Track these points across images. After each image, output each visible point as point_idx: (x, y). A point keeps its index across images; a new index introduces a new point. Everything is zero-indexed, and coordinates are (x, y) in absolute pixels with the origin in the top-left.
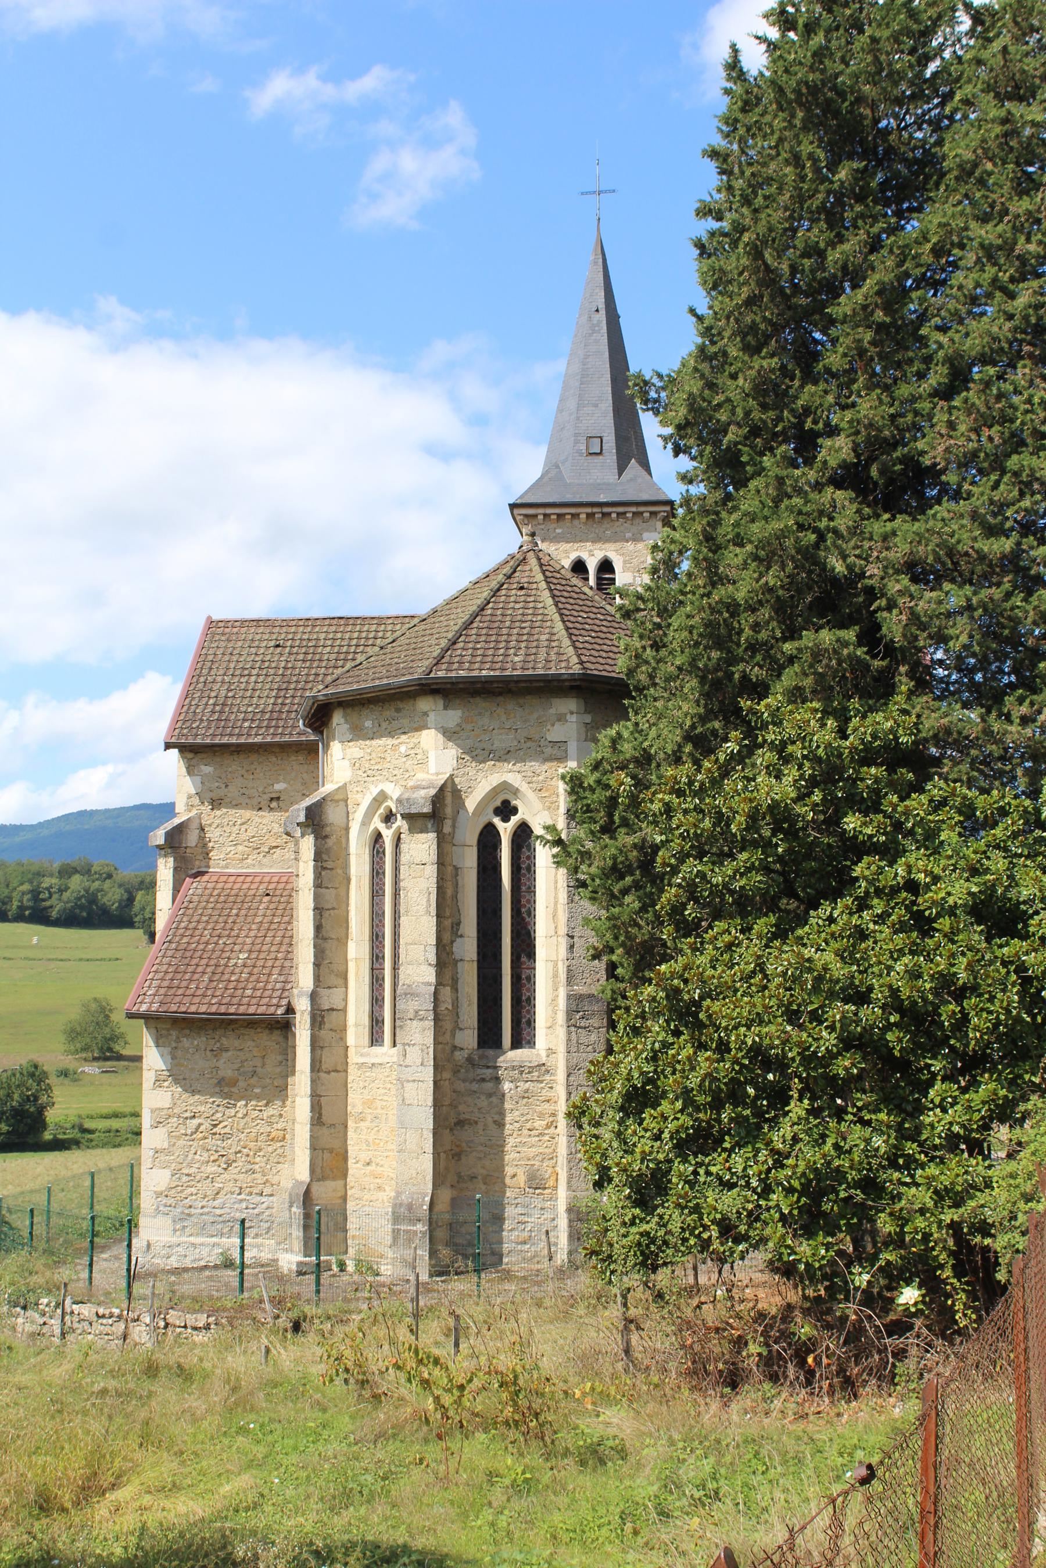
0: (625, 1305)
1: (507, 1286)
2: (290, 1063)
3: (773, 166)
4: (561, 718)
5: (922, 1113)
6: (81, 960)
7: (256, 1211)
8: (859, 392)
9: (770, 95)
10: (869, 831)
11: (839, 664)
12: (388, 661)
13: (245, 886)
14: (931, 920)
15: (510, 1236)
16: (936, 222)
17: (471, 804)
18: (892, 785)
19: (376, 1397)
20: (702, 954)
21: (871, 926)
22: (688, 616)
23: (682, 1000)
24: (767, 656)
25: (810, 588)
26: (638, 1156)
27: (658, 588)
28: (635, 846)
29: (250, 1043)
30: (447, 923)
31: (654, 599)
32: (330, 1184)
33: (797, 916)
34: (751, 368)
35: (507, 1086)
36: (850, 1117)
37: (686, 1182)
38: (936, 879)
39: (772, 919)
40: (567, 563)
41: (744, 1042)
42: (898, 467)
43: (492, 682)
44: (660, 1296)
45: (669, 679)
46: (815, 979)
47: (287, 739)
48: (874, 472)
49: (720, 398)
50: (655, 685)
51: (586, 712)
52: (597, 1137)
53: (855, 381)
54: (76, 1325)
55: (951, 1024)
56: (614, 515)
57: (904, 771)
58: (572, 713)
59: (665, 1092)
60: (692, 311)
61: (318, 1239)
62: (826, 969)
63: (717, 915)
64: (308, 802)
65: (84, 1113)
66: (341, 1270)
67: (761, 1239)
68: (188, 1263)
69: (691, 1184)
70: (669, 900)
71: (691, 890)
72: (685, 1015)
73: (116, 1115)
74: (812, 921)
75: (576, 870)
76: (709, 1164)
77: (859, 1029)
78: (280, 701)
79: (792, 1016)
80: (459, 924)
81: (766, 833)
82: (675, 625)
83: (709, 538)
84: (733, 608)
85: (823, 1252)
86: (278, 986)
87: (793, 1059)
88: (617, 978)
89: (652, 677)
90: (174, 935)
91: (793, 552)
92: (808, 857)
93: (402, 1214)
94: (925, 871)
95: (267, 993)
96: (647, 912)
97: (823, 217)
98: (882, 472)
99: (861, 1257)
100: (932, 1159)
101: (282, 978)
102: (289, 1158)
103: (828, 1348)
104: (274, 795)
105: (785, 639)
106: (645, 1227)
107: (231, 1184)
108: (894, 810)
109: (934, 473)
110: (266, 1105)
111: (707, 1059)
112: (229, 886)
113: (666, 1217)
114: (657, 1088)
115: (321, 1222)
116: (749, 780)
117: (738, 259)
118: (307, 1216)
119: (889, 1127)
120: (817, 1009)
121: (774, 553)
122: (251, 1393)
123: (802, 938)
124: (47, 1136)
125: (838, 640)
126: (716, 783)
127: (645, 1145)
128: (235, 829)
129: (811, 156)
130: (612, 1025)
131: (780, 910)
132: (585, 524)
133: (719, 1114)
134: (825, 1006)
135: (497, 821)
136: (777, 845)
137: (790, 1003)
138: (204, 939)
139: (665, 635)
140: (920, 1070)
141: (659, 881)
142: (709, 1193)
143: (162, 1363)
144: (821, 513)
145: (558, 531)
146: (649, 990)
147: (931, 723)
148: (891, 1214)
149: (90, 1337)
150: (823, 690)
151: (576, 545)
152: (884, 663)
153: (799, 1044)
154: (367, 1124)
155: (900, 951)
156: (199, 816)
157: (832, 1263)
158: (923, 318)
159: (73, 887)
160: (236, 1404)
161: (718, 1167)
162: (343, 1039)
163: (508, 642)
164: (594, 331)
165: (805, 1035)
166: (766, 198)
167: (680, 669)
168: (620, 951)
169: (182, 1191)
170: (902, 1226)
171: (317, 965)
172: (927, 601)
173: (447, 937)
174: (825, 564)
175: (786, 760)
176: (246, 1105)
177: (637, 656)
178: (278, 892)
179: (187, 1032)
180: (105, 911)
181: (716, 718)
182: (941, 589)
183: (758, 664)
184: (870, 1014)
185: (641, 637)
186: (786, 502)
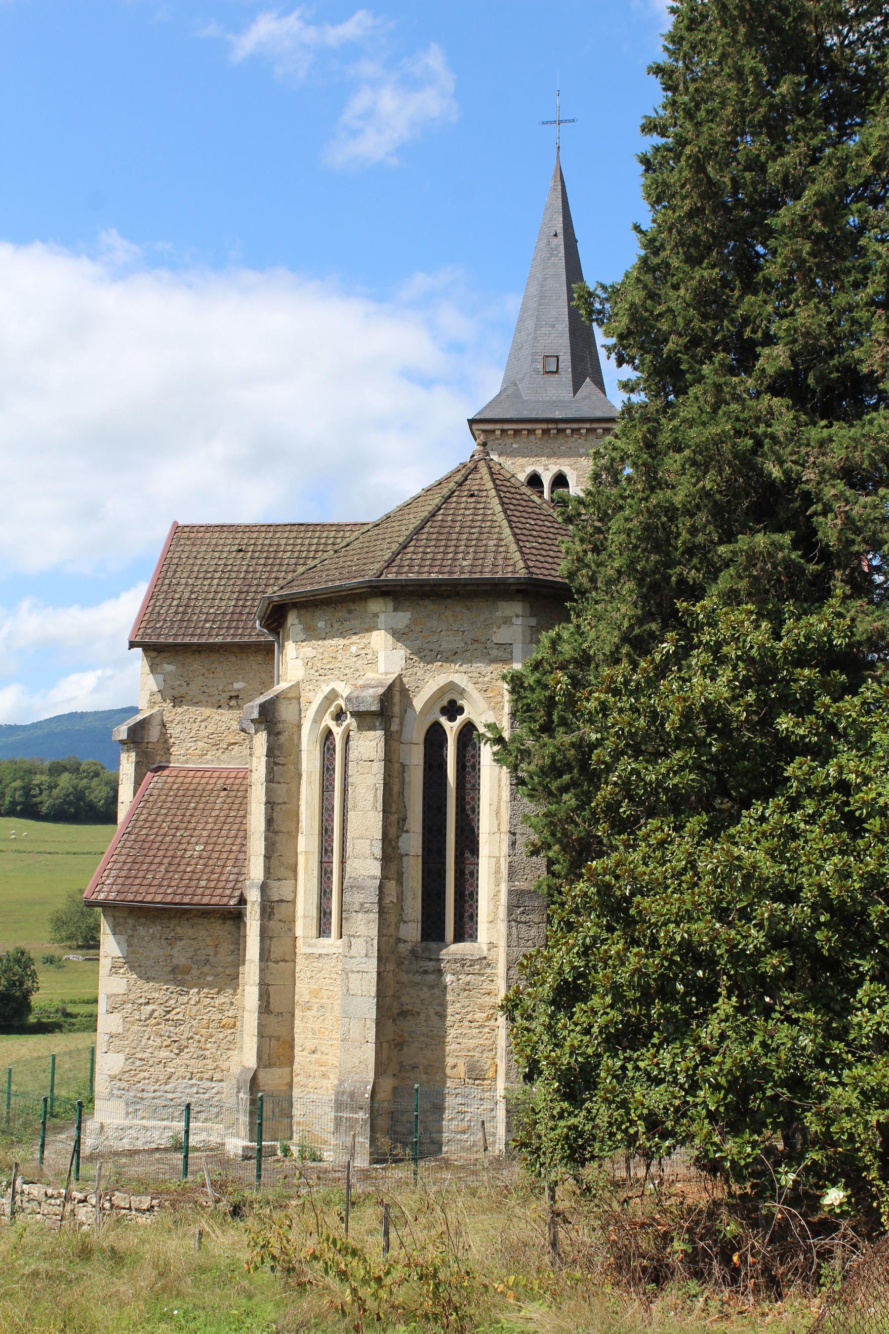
0: (552, 1198)
2: (241, 953)
3: (716, 82)
4: (507, 621)
5: (850, 1013)
6: (68, 853)
7: (206, 1096)
8: (797, 300)
9: (714, 12)
10: (801, 731)
11: (775, 566)
12: (341, 564)
13: (204, 781)
14: (862, 821)
15: (450, 1124)
16: (877, 135)
17: (418, 703)
18: (826, 687)
19: (301, 1285)
20: (635, 850)
21: (802, 825)
22: (627, 520)
23: (613, 896)
24: (704, 558)
25: (748, 495)
26: (567, 1050)
27: (598, 492)
28: (573, 744)
29: (203, 932)
30: (394, 818)
31: (594, 503)
32: (277, 1071)
33: (731, 816)
34: (692, 278)
35: (449, 978)
36: (777, 1015)
37: (614, 1077)
38: (867, 780)
40: (522, 477)
41: (674, 939)
42: (835, 375)
43: (440, 585)
45: (609, 582)
46: (744, 877)
47: (246, 639)
48: (811, 381)
49: (663, 308)
50: (596, 588)
51: (531, 615)
52: (528, 1030)
53: (794, 290)
54: (25, 1205)
55: (880, 925)
56: (569, 432)
57: (836, 672)
58: (517, 616)
59: (594, 986)
60: (637, 228)
61: (260, 1124)
62: (754, 867)
64: (262, 699)
65: (67, 998)
66: (286, 1156)
67: (687, 1136)
68: (139, 1145)
69: (619, 1079)
70: (604, 798)
71: (625, 785)
72: (617, 911)
74: (745, 820)
76: (637, 1059)
77: (787, 928)
78: (241, 603)
79: (721, 914)
80: (404, 819)
82: (614, 528)
83: (649, 446)
84: (671, 512)
85: (749, 1150)
86: (232, 877)
87: (721, 956)
89: (593, 579)
90: (134, 827)
91: (730, 457)
92: (741, 757)
94: (856, 772)
95: (222, 884)
96: (585, 810)
97: (764, 130)
98: (819, 379)
99: (792, 1157)
100: (859, 1059)
101: (236, 870)
102: (238, 1045)
103: (753, 1247)
104: (233, 694)
105: (721, 542)
106: (573, 1121)
107: (182, 1069)
108: (827, 711)
109: (872, 380)
110: (218, 993)
111: (636, 955)
112: (188, 780)
113: (594, 1111)
114: (588, 982)
115: (266, 1107)
116: (685, 681)
117: (680, 172)
118: (253, 1102)
119: (816, 1026)
120: (746, 907)
121: (711, 458)
122: (179, 1278)
123: (734, 837)
124: (32, 1019)
125: (773, 543)
126: (651, 684)
127: (574, 1039)
128: (195, 726)
129: (753, 71)
131: (715, 809)
132: (541, 439)
133: (649, 1011)
134: (754, 904)
135: (443, 720)
136: (711, 744)
137: (720, 901)
138: (162, 831)
139: (606, 539)
140: (849, 970)
141: (595, 778)
142: (638, 1088)
143: (95, 1247)
144: (758, 419)
145: (515, 446)
146: (581, 886)
147: (866, 626)
148: (817, 1114)
149: (38, 1217)
150: (757, 593)
151: (532, 460)
152: (819, 567)
153: (728, 941)
154: (313, 1013)
155: (830, 850)
156: (161, 713)
158: (862, 229)
159: (52, 784)
160: (164, 1289)
161: (646, 1062)
162: (292, 930)
163: (456, 547)
164: (552, 255)
165: (733, 932)
166: (708, 112)
167: (619, 572)
168: (556, 847)
169: (135, 1075)
170: (828, 1126)
171: (267, 857)
172: (862, 505)
173: (393, 832)
174: (762, 469)
175: (722, 660)
176: (199, 993)
177: (579, 560)
178: (235, 787)
179: (143, 920)
180: (91, 807)
181: (654, 620)
182: (876, 494)
183: (695, 567)
184: (798, 913)
185: (582, 540)
186: (724, 408)
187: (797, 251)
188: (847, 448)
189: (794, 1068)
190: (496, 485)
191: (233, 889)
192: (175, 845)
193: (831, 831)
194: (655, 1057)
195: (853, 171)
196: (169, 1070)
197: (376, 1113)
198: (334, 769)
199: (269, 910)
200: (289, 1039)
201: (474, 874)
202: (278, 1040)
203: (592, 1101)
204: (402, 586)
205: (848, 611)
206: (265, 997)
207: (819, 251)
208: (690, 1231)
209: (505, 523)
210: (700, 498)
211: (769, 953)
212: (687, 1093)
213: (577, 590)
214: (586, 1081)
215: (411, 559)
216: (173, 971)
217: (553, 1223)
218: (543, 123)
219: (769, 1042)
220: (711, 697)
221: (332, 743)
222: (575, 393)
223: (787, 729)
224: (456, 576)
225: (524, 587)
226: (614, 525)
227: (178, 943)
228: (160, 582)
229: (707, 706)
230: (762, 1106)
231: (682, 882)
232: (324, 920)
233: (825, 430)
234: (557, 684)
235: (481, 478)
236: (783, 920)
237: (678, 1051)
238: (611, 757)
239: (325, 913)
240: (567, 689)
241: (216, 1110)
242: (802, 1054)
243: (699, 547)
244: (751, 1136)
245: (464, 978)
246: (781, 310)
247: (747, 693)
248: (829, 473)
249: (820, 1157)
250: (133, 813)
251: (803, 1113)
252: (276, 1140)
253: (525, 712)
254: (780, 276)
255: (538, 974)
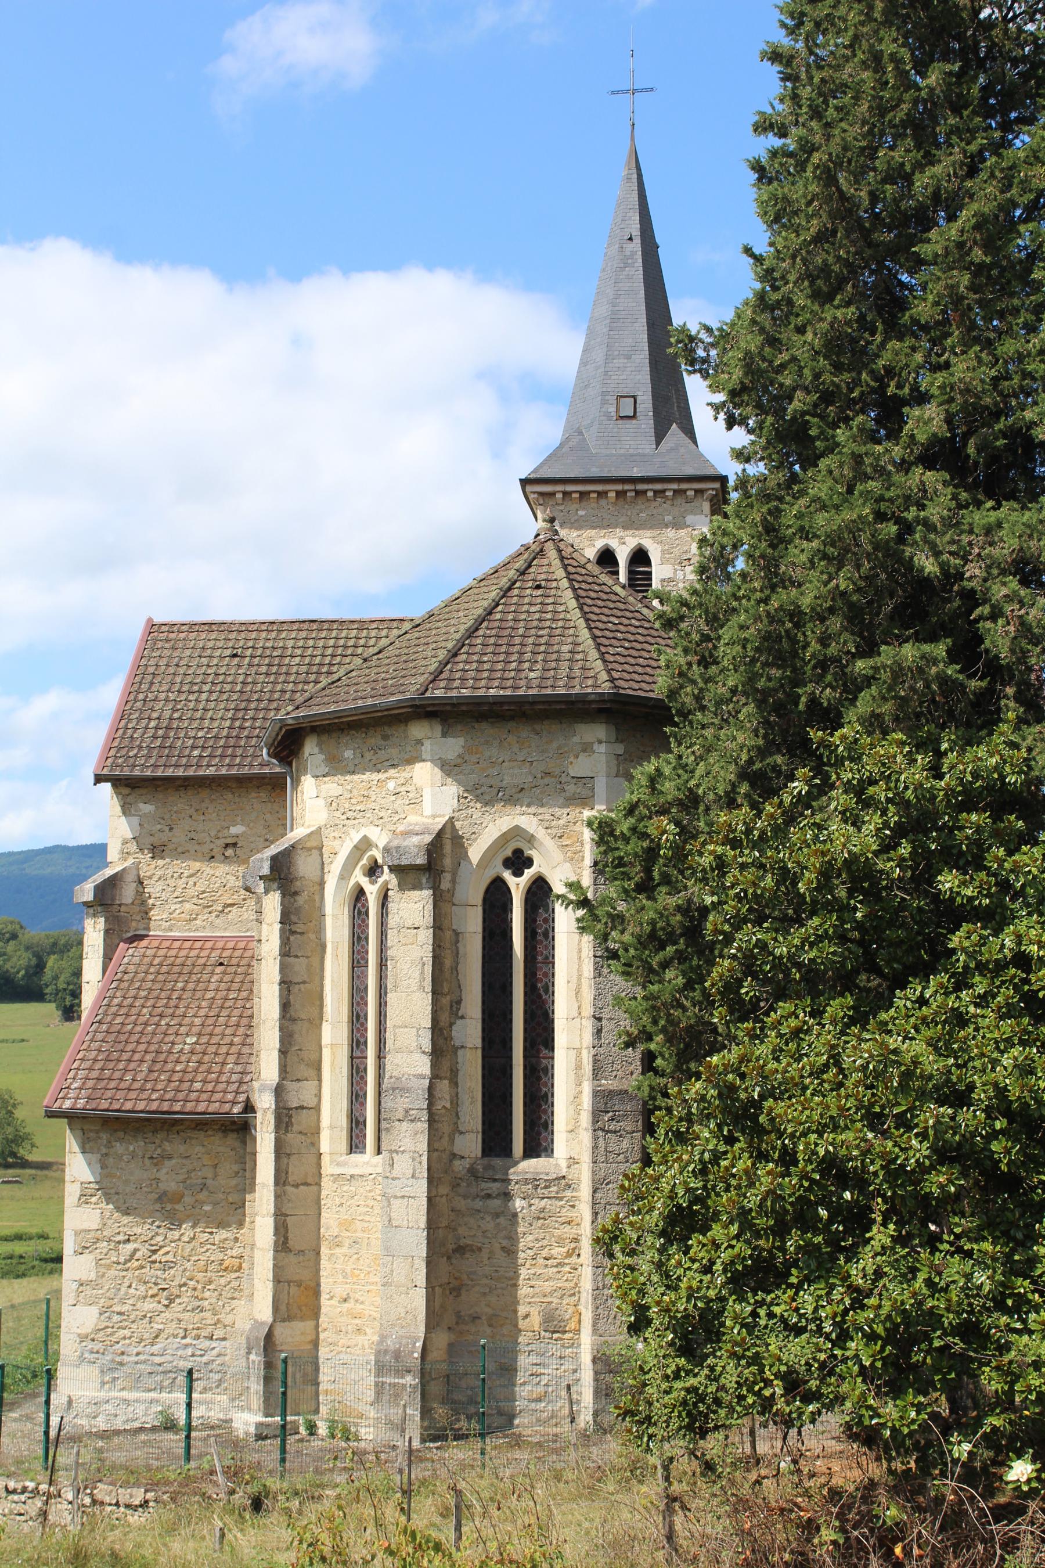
1: (518, 1454)
3: (848, 70)
4: (587, 748)
8: (953, 347)
10: (969, 892)
11: (927, 686)
12: (373, 677)
13: (193, 953)
15: (524, 1392)
17: (475, 853)
18: (996, 834)
20: (762, 1042)
21: (972, 1009)
22: (742, 627)
23: (738, 1099)
26: (683, 1293)
27: (706, 591)
28: (678, 908)
29: (198, 1149)
30: (445, 1001)
31: (701, 605)
32: (298, 1326)
34: (821, 319)
35: (518, 1203)
36: (946, 1246)
37: (743, 1325)
39: (850, 1000)
40: (591, 553)
43: (502, 704)
44: (709, 1467)
47: (245, 771)
48: (971, 450)
49: (785, 357)
51: (617, 741)
56: (650, 494)
57: (1013, 817)
58: (600, 742)
60: (748, 251)
61: (284, 1394)
62: (916, 1063)
63: (781, 994)
64: (273, 850)
66: (311, 1434)
67: (836, 1397)
68: (119, 1424)
69: (750, 1328)
70: (721, 976)
71: (748, 965)
72: (742, 1118)
73: (19, 1237)
74: (899, 1002)
75: (605, 937)
76: (771, 1304)
77: (957, 1138)
78: (237, 724)
79: (874, 1120)
80: (459, 1002)
81: (842, 893)
82: (726, 639)
84: (796, 616)
85: (913, 1414)
86: (235, 1078)
87: (875, 1174)
88: (656, 1072)
89: (698, 698)
90: (105, 1014)
92: (891, 924)
93: (387, 1363)
99: (961, 1421)
101: (239, 1068)
102: (246, 1292)
103: (920, 1535)
104: (229, 841)
106: (692, 1381)
107: (174, 1325)
111: (769, 1173)
112: (173, 953)
113: (719, 1369)
116: (820, 827)
118: (268, 1365)
119: (994, 1259)
120: (905, 1112)
121: (847, 550)
123: (886, 1024)
126: (780, 832)
127: (691, 1279)
128: (181, 883)
130: (650, 1129)
132: (615, 504)
133: (784, 1243)
134: (915, 1108)
135: (507, 875)
136: (855, 909)
137: (872, 1105)
138: (142, 1019)
141: (708, 953)
142: (772, 1340)
145: (581, 513)
146: (697, 1086)
153: (883, 1155)
154: (344, 1250)
155: (1008, 1040)
156: (137, 866)
157: (924, 1428)
161: (783, 1307)
162: (315, 1144)
163: (521, 653)
165: (890, 1144)
169: (112, 1334)
170: (1012, 1384)
171: (283, 1052)
173: (444, 1018)
175: (867, 803)
177: (681, 674)
178: (234, 961)
179: (121, 1134)
183: (830, 685)
184: (970, 1118)
185: (686, 651)
187: (952, 286)
188: (1020, 536)
189: (968, 1312)
190: (568, 573)
191: (237, 1092)
192: (158, 1037)
193: (1008, 1015)
194: (794, 1300)
195: (1022, 182)
196: (156, 1326)
197: (427, 1377)
198: (367, 939)
199: (286, 1119)
200: (313, 1284)
201: (548, 1071)
202: (299, 1286)
203: (715, 1357)
204: (453, 705)
205: (1024, 740)
206: (282, 1230)
207: (980, 286)
208: (840, 1516)
209: (582, 623)
210: (833, 599)
211: (935, 1169)
212: (833, 1346)
213: (677, 711)
214: (708, 1331)
215: (463, 670)
216: (160, 1199)
217: (669, 1511)
218: (613, 93)
219: (937, 1280)
220: (855, 849)
221: (363, 906)
222: (658, 444)
223: (951, 889)
224: (521, 692)
225: (608, 705)
226: (727, 633)
227: (167, 1163)
228: (132, 697)
229: (854, 858)
230: (929, 1360)
231: (823, 1081)
232: (356, 1131)
233: (992, 513)
234: (662, 834)
235: (549, 565)
236: (952, 1128)
237: (823, 1292)
238: (731, 925)
239: (357, 1123)
240: (675, 841)
241: (217, 1377)
242: (978, 1295)
243: (836, 660)
244: (915, 1397)
245: (539, 1204)
246: (934, 359)
247: (900, 845)
248: (998, 567)
249: (1001, 1422)
250: (104, 998)
251: (979, 1368)
252: (299, 1414)
253: (616, 867)
254: (932, 317)
255: (643, 1199)
